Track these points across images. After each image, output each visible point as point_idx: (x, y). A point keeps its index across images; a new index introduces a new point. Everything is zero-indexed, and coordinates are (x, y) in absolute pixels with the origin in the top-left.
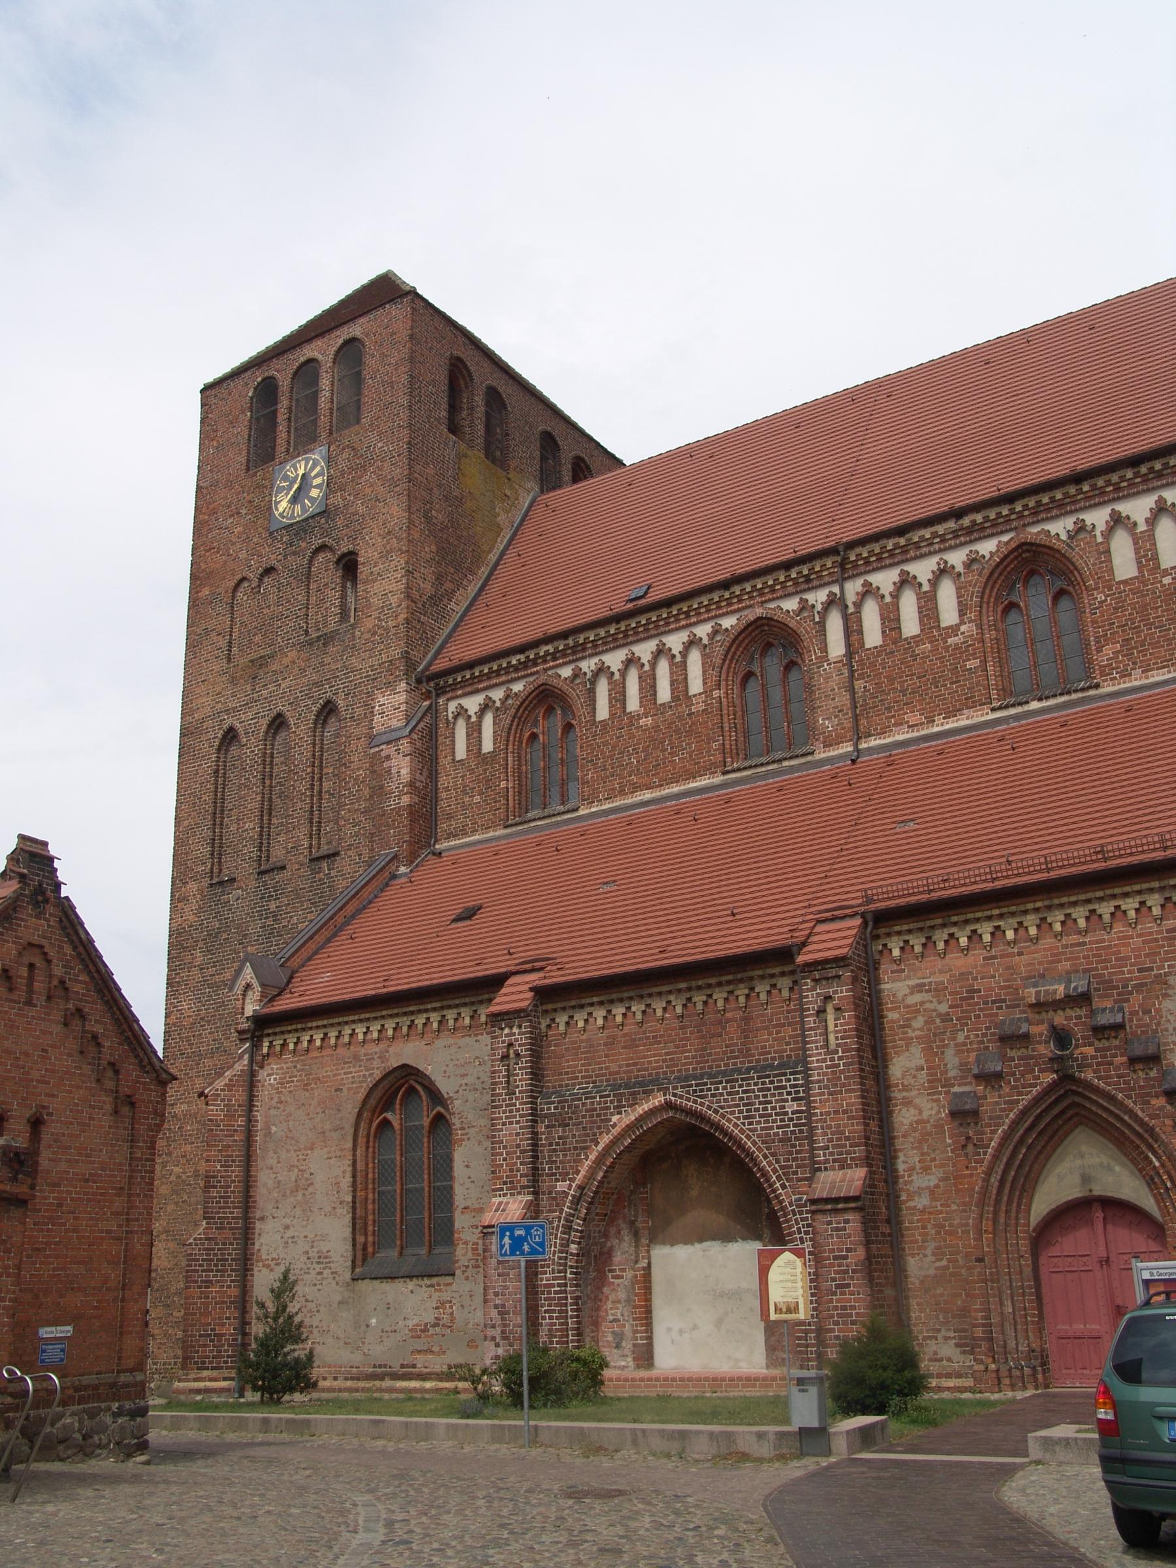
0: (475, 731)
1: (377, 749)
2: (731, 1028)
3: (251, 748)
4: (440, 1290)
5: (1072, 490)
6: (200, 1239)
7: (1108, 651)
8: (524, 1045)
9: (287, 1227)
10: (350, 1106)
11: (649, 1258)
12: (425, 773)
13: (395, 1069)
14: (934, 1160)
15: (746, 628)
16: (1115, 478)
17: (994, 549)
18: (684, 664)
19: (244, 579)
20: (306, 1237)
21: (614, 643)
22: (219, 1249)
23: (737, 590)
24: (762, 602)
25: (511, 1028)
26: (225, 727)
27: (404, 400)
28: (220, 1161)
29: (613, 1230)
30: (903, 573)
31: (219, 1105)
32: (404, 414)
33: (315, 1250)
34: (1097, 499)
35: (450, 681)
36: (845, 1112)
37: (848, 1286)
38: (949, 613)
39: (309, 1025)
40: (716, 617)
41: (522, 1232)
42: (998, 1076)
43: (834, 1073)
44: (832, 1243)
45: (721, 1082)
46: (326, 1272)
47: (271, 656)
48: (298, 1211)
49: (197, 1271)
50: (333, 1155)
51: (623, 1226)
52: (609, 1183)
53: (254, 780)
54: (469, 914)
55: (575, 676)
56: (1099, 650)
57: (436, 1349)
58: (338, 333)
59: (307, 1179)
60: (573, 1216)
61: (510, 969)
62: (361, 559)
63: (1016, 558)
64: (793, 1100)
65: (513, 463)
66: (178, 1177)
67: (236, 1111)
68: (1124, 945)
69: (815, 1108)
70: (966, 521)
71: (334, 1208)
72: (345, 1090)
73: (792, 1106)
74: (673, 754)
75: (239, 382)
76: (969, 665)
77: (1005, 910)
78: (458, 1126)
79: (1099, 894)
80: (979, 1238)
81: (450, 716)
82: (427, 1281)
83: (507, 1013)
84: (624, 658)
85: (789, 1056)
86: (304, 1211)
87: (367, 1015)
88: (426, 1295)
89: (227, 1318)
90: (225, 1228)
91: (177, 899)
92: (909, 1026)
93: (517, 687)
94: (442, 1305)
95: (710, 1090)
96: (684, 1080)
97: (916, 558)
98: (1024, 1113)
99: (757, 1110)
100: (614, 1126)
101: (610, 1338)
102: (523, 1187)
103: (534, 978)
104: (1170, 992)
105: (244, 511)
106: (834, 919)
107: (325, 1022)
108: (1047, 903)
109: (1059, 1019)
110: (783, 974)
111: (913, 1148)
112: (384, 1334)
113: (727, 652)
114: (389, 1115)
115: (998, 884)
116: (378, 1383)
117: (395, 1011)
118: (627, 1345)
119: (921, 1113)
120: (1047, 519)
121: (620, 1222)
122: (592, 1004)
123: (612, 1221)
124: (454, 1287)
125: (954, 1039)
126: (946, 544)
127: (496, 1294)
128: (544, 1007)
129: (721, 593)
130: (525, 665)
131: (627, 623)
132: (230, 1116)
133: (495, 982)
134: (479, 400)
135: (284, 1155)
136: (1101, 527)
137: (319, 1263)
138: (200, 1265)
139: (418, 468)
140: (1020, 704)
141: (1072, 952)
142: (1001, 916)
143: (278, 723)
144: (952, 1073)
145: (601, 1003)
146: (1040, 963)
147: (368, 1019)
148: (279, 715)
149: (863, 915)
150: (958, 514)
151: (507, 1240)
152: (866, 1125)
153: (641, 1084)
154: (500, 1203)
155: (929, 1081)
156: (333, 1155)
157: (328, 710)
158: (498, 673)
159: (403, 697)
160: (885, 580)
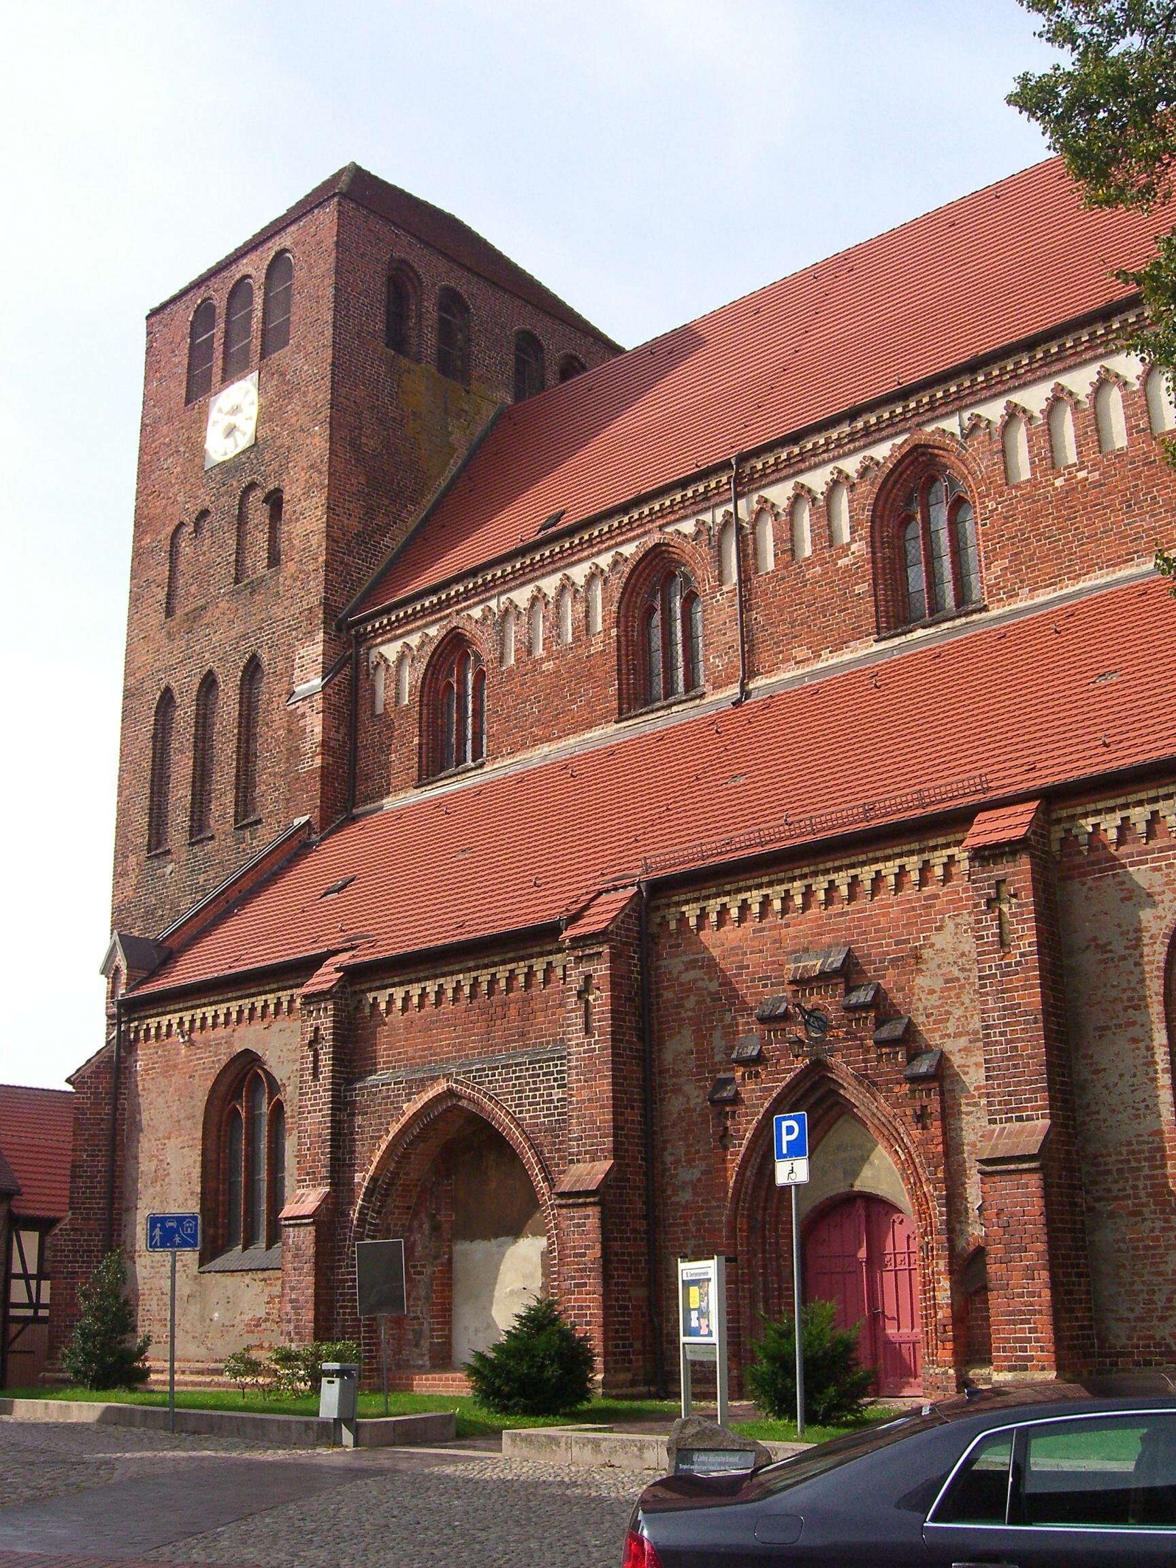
1: (294, 707)
3: (185, 712)
7: (996, 568)
10: (200, 1094)
11: (451, 1253)
12: (343, 730)
14: (698, 1152)
17: (887, 454)
19: (182, 524)
22: (85, 1240)
27: (329, 316)
28: (86, 1150)
29: (416, 1224)
32: (329, 332)
36: (598, 1100)
37: (585, 1284)
41: (173, 1224)
43: (590, 1058)
44: (574, 1239)
47: (203, 608)
49: (62, 1262)
51: (425, 1219)
53: (187, 744)
58: (270, 244)
60: (368, 1208)
61: (337, 946)
62: (286, 497)
63: (912, 463)
65: (475, 374)
67: (104, 1099)
68: (884, 915)
74: (573, 701)
75: (181, 305)
76: (858, 589)
77: (774, 877)
78: (289, 1114)
79: (862, 857)
82: (260, 1275)
87: (216, 998)
91: (120, 874)
92: (682, 1006)
93: (433, 631)
95: (487, 1076)
97: (810, 469)
99: (527, 1097)
102: (323, 1178)
103: (343, 958)
104: (924, 967)
105: (182, 449)
107: (181, 1006)
108: (812, 868)
111: (680, 1139)
116: (216, 1378)
118: (425, 1344)
119: (688, 1102)
123: (415, 1215)
125: (722, 1020)
126: (841, 449)
130: (434, 609)
133: (311, 965)
134: (430, 306)
138: (66, 1256)
139: (343, 391)
140: (905, 633)
141: (835, 923)
143: (209, 683)
146: (805, 936)
148: (210, 672)
151: (157, 1232)
155: (698, 1067)
157: (253, 669)
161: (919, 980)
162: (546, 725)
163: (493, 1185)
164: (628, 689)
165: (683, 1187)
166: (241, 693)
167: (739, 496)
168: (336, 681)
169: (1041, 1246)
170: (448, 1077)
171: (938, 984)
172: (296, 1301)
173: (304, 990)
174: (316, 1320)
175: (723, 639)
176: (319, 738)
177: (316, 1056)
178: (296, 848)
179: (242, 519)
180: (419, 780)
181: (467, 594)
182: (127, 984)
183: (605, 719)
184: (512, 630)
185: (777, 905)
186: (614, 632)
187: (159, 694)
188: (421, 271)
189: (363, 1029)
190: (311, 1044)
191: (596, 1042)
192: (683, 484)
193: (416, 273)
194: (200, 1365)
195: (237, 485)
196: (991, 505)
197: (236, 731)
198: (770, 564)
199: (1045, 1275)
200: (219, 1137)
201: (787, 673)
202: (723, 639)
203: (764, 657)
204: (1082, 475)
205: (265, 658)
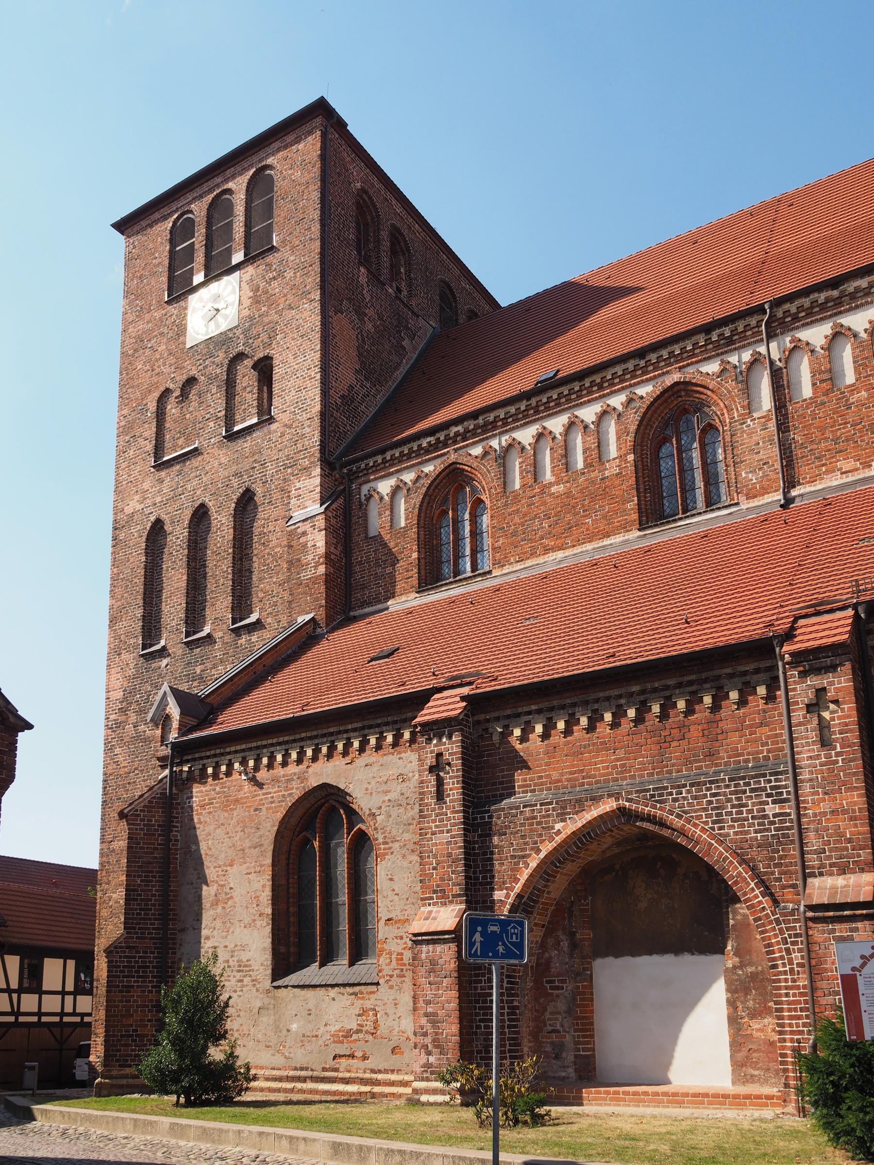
2: (695, 732)
3: (178, 537)
4: (363, 998)
6: (121, 947)
8: (455, 753)
10: (269, 825)
12: (340, 548)
20: (226, 947)
21: (523, 419)
22: (140, 957)
23: (653, 357)
24: (680, 368)
25: (440, 739)
28: (140, 876)
30: (836, 325)
31: (139, 825)
33: (235, 959)
35: (363, 466)
39: (228, 750)
40: (631, 386)
45: (684, 786)
49: (119, 977)
50: (252, 870)
51: (563, 937)
52: (549, 893)
55: (486, 454)
57: (359, 1054)
59: (226, 894)
62: (275, 362)
64: (774, 802)
67: (157, 830)
69: (806, 808)
71: (254, 920)
72: (264, 809)
73: (771, 809)
78: (381, 840)
81: (363, 498)
82: (349, 990)
85: (766, 758)
86: (224, 923)
88: (348, 1003)
89: (149, 1021)
90: (146, 938)
93: (429, 468)
94: (363, 1012)
100: (559, 832)
102: (454, 896)
103: (465, 691)
107: (244, 747)
112: (305, 1039)
116: (299, 1085)
117: (315, 733)
121: (560, 933)
122: (529, 713)
124: (379, 995)
128: (476, 718)
129: (636, 361)
131: (538, 399)
133: (422, 698)
137: (239, 971)
138: (121, 972)
145: (539, 712)
147: (287, 742)
148: (202, 505)
149: (855, 607)
151: (478, 937)
154: (430, 912)
156: (252, 870)
157: (246, 503)
158: (409, 457)
159: (318, 480)
160: (816, 335)
162: (557, 537)
163: (643, 905)
164: (646, 505)
166: (235, 521)
168: (334, 506)
172: (435, 1014)
175: (757, 457)
177: (440, 783)
178: (303, 641)
179: (230, 385)
180: (419, 587)
182: (179, 729)
183: (625, 528)
186: (631, 457)
187: (150, 524)
189: (488, 755)
190: (431, 769)
191: (838, 754)
194: (275, 1073)
195: (222, 357)
197: (231, 551)
198: (807, 391)
200: (288, 864)
201: (836, 480)
203: (803, 469)
205: (259, 490)
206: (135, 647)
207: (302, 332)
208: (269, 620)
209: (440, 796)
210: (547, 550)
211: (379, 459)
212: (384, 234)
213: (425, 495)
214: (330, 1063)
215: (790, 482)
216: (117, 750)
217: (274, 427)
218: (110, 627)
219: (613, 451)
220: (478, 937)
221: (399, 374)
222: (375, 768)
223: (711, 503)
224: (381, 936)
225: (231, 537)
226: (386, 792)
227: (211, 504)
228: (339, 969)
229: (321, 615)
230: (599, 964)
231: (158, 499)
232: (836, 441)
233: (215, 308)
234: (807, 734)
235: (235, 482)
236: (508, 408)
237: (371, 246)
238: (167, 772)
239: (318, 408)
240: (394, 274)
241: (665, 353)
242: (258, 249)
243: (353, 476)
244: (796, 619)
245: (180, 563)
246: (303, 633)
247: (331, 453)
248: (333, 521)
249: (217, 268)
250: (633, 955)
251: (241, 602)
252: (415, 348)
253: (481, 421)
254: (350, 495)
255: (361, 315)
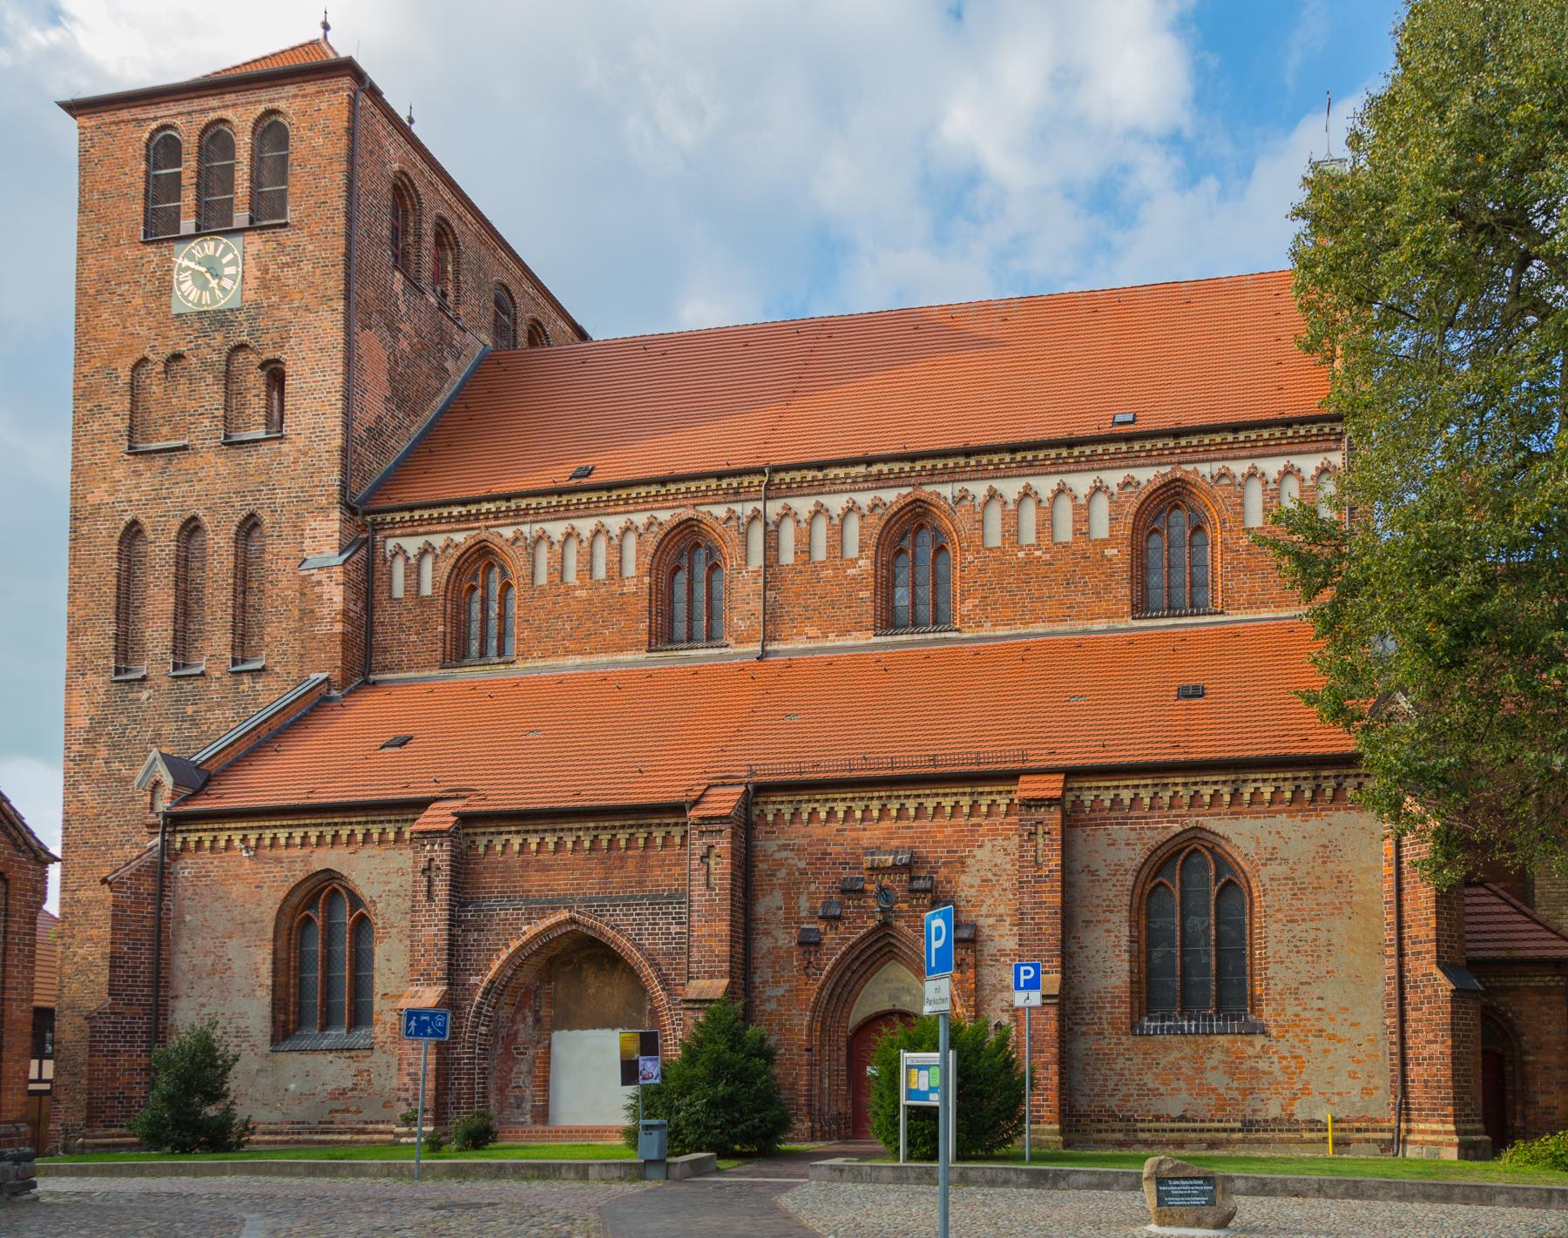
0: (414, 572)
2: (631, 864)
3: (161, 548)
5: (962, 461)
7: (969, 603)
9: (203, 1005)
12: (360, 604)
13: (318, 873)
15: (678, 525)
16: (996, 459)
18: (621, 548)
21: (555, 514)
23: (673, 488)
26: (128, 518)
29: (519, 1017)
34: (980, 474)
38: (1101, 529)
42: (838, 918)
46: (244, 1045)
48: (215, 992)
54: (403, 742)
56: (962, 602)
57: (353, 1108)
66: (84, 958)
70: (874, 469)
73: (674, 929)
76: (861, 595)
80: (810, 1035)
83: (429, 832)
84: (1120, 481)
93: (459, 538)
94: (359, 1073)
96: (588, 901)
98: (852, 947)
101: (512, 1100)
103: (458, 805)
106: (724, 785)
109: (886, 881)
110: (676, 824)
113: (660, 544)
114: (310, 913)
115: (855, 774)
118: (528, 1106)
120: (1135, 466)
123: (519, 1009)
124: (373, 1058)
126: (855, 485)
127: (410, 1065)
129: (658, 488)
132: (138, 903)
133: (421, 805)
135: (199, 942)
136: (980, 499)
142: (853, 799)
143: (191, 527)
144: (803, 914)
150: (869, 462)
151: (413, 1023)
152: (732, 947)
153: (550, 902)
157: (250, 525)
159: (337, 526)
161: (963, 878)
163: (592, 991)
165: (769, 999)
167: (767, 498)
168: (354, 558)
169: (1055, 1050)
170: (571, 909)
171: (977, 882)
173: (415, 827)
174: (437, 1089)
175: (747, 607)
176: (339, 606)
181: (497, 514)
183: (635, 646)
184: (543, 553)
185: (858, 814)
186: (647, 580)
188: (421, 191)
190: (424, 871)
192: (720, 476)
193: (416, 191)
196: (970, 558)
199: (1055, 1068)
201: (801, 644)
202: (747, 607)
204: (1038, 553)
205: (267, 519)
206: (106, 669)
207: (322, 343)
208: (277, 669)
209: (430, 896)
210: (567, 652)
211: (407, 516)
212: (428, 228)
213: (454, 567)
214: (327, 1117)
215: (768, 638)
216: (82, 787)
217: (286, 447)
218: (70, 640)
219: (630, 569)
220: (413, 1023)
221: (439, 402)
222: (377, 861)
223: (711, 638)
224: (376, 1008)
225: (231, 565)
226: (387, 883)
227: (205, 519)
228: (338, 1034)
229: (337, 675)
230: (556, 1035)
231: (135, 496)
232: (806, 608)
233: (209, 275)
234: (699, 878)
235: (236, 500)
236: (540, 499)
237: (411, 239)
238: (158, 840)
239: (338, 442)
240: (439, 276)
241: (683, 487)
242: (268, 213)
243: (376, 527)
244: (710, 787)
245: (165, 581)
246: (316, 694)
247: (353, 495)
248: (353, 575)
249: (214, 222)
250: (582, 1029)
251: (243, 639)
252: (459, 370)
253: (513, 504)
254: (374, 546)
255: (393, 330)
